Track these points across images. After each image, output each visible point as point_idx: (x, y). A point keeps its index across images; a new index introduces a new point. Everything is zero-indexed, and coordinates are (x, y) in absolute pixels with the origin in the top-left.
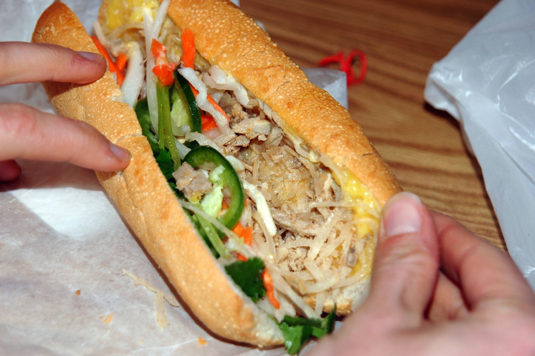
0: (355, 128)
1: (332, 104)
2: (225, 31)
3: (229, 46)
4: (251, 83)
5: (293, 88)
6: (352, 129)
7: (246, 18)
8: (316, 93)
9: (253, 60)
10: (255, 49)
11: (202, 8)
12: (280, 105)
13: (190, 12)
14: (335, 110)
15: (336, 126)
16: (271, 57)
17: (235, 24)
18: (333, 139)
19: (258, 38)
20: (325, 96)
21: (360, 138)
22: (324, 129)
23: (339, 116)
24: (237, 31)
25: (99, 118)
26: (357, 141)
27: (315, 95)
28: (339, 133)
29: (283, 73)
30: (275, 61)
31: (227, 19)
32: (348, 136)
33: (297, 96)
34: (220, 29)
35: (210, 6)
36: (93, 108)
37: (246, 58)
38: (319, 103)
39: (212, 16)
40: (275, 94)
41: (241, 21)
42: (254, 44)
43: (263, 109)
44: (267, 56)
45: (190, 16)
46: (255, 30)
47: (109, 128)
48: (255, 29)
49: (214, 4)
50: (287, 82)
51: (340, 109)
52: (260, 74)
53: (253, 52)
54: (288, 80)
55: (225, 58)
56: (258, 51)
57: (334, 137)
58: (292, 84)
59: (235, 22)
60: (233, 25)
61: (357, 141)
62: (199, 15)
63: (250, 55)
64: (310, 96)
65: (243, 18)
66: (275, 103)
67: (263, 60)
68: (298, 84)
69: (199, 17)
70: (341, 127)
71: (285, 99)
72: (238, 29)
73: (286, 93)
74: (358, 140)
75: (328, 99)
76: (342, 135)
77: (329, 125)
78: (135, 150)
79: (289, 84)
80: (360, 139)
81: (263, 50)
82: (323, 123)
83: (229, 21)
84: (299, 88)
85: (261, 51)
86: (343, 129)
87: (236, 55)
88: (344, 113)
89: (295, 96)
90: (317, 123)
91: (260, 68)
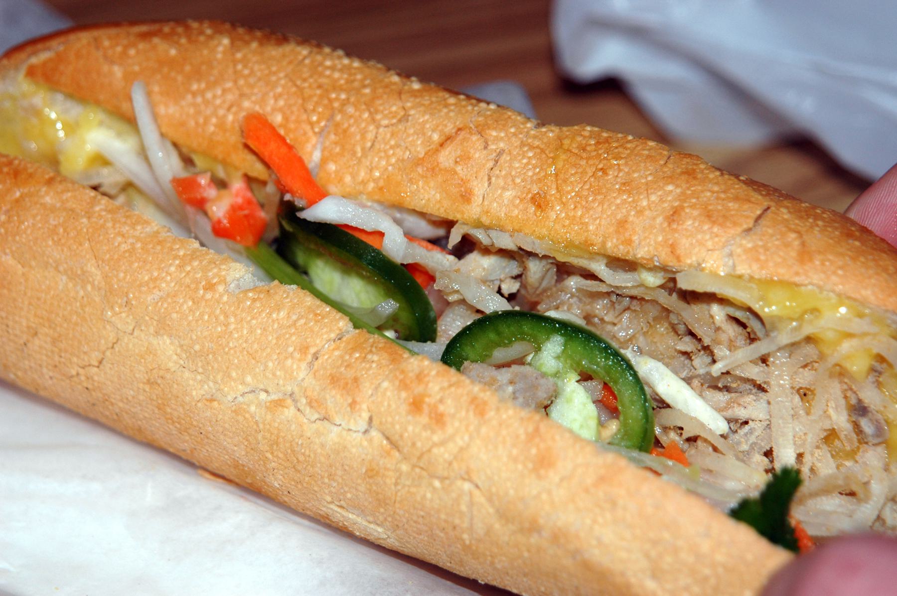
0: (698, 171)
1: (616, 148)
2: (295, 109)
3: (327, 143)
4: (426, 198)
5: (520, 161)
6: (695, 178)
7: (319, 58)
8: (570, 145)
9: (398, 146)
10: (385, 122)
11: (216, 83)
12: (519, 213)
13: (194, 105)
14: (633, 157)
15: (660, 193)
16: (430, 120)
17: (306, 85)
18: (675, 226)
19: (374, 91)
20: (590, 137)
21: (723, 187)
22: (640, 212)
23: (648, 164)
24: (321, 97)
25: (228, 343)
26: (723, 200)
27: (570, 148)
28: (676, 204)
29: (478, 140)
30: (444, 123)
31: (283, 82)
32: (698, 198)
33: (539, 172)
34: (281, 110)
35: (230, 71)
36: (199, 329)
37: (379, 151)
38: (591, 162)
39: (246, 90)
40: (491, 195)
41: (315, 70)
42: (377, 111)
43: (493, 242)
44: (421, 120)
45: (198, 113)
46: (355, 74)
47: (269, 350)
48: (353, 71)
49: (235, 62)
50: (501, 153)
51: (639, 148)
52: (433, 169)
53: (386, 129)
54: (498, 151)
55: (336, 172)
56: (394, 121)
57: (674, 221)
58: (510, 153)
59: (305, 80)
60: (304, 88)
61: (723, 200)
62: (218, 102)
63: (384, 139)
64: (563, 157)
65: (313, 62)
66: (505, 214)
67: (418, 135)
68: (523, 144)
69: (220, 106)
70: (670, 188)
71: (519, 193)
72: (318, 92)
73: (513, 180)
74: (723, 196)
75: (600, 141)
76: (686, 205)
77: (644, 198)
78: (368, 366)
79: (505, 157)
80: (724, 192)
81: (402, 113)
82: (630, 200)
83: (290, 84)
84: (531, 154)
85: (399, 117)
86: (679, 190)
87: (354, 153)
88: (653, 153)
89: (535, 178)
90: (618, 207)
91: (424, 157)
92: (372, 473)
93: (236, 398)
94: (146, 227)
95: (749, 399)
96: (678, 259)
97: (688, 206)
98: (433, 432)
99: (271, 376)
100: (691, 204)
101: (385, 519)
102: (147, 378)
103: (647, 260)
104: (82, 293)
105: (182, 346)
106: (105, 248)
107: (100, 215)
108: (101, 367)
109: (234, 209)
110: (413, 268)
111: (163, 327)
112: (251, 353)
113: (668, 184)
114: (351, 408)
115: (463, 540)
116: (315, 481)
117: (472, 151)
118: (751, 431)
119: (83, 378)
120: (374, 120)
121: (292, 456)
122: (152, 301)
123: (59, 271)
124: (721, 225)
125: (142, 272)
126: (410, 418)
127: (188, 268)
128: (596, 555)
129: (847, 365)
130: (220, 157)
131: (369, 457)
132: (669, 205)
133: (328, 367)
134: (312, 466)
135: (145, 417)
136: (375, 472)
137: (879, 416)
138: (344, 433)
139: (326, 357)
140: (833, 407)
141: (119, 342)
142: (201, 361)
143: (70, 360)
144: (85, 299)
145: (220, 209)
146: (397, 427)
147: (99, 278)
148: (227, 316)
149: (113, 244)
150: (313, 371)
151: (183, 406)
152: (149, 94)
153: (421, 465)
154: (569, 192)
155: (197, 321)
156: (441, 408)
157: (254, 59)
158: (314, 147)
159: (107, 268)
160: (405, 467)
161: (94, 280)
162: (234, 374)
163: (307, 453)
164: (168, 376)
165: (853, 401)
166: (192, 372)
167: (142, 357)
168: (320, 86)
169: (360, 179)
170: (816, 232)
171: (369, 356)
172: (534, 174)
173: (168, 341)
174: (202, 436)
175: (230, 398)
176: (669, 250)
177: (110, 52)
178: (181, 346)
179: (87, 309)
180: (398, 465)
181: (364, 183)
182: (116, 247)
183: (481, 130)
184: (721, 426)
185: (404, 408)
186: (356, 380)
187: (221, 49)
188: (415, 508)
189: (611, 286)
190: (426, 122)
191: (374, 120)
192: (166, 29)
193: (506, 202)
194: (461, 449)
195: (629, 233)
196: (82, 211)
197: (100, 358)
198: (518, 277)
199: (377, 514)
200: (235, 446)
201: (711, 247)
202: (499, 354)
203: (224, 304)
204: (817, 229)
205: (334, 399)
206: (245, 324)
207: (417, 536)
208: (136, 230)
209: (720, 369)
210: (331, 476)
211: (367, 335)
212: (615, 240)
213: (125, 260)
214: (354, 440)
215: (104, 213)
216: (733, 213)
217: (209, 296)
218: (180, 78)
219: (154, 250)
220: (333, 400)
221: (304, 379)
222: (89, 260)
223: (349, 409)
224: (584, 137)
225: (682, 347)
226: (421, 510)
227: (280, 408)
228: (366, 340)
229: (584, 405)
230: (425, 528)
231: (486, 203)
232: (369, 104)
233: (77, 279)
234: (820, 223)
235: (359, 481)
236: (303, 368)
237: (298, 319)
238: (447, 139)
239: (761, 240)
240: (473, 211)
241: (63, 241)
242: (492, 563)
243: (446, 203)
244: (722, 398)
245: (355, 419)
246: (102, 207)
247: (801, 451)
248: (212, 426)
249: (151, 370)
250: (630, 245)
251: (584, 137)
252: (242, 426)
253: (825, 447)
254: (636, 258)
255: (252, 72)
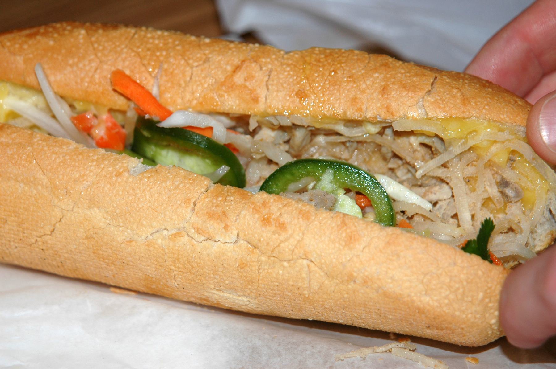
1: (338, 57)
6: (389, 67)
17: (140, 50)
28: (383, 84)
31: (125, 50)
32: (395, 78)
39: (103, 59)
42: (189, 59)
49: (92, 43)
50: (271, 71)
52: (232, 87)
55: (171, 98)
57: (384, 93)
58: (276, 70)
59: (138, 47)
61: (410, 77)
62: (87, 68)
68: (282, 64)
70: (376, 75)
72: (149, 53)
74: (408, 74)
76: (389, 83)
79: (274, 73)
80: (408, 72)
81: (204, 57)
83: (130, 51)
86: (382, 76)
87: (180, 85)
89: (295, 82)
92: (243, 265)
93: (147, 237)
94: (70, 146)
95: (437, 188)
96: (393, 114)
97: (391, 84)
98: (279, 235)
99: (169, 220)
100: (392, 82)
101: (251, 292)
102: (85, 235)
103: (373, 118)
104: (35, 192)
105: (107, 212)
106: (47, 162)
107: (38, 144)
108: (53, 234)
109: (109, 129)
110: (228, 146)
111: (93, 203)
112: (154, 208)
113: (375, 73)
114: (225, 230)
115: (304, 295)
116: (204, 278)
117: (254, 73)
118: (441, 207)
119: (40, 243)
120: (188, 64)
121: (189, 265)
122: (84, 188)
123: (18, 181)
124: (414, 91)
125: (74, 173)
126: (263, 229)
127: (102, 166)
128: (391, 287)
129: (496, 160)
130: (94, 100)
131: (240, 256)
132: (379, 85)
133: (205, 209)
134: (202, 269)
135: (83, 260)
136: (245, 265)
137: (517, 185)
138: (222, 245)
139: (201, 203)
140: (488, 185)
141: (64, 217)
142: (121, 219)
143: (31, 233)
144: (38, 195)
145: (100, 132)
146: (256, 235)
147: (46, 180)
148: (134, 190)
149: (51, 159)
150: (195, 212)
151: (111, 249)
152: (43, 69)
153: (274, 255)
154: (318, 87)
155: (115, 196)
156: (282, 220)
157: (104, 40)
158: (153, 85)
159: (50, 174)
160: (263, 258)
161: (42, 182)
162: (144, 223)
163: (199, 261)
164: (100, 232)
165: (499, 180)
166: (116, 226)
167: (81, 223)
168: (149, 50)
169: (187, 99)
170: (467, 87)
171: (228, 198)
172: (294, 80)
173: (98, 211)
174: (124, 264)
175: (143, 238)
176: (385, 110)
177: (12, 49)
178: (107, 212)
179: (40, 201)
180: (260, 258)
181: (190, 101)
182: (53, 161)
183: (256, 60)
184: (429, 206)
185: (258, 224)
186: (224, 213)
187: (81, 37)
188: (271, 281)
189: (348, 137)
190: (221, 60)
191: (188, 64)
192: (42, 30)
193: (281, 98)
194: (299, 241)
195: (359, 105)
196: (26, 143)
197: (52, 229)
198: (287, 142)
199: (246, 290)
200: (148, 266)
201: (410, 105)
202: (292, 186)
203: (130, 183)
204: (466, 85)
205: (213, 227)
206: (147, 193)
207: (272, 298)
208: (64, 149)
209: (421, 173)
210: (215, 273)
211: (222, 186)
212: (351, 110)
213: (61, 167)
214: (229, 248)
215: (40, 142)
216: (417, 83)
217: (119, 180)
218: (60, 58)
219: (78, 159)
220: (212, 227)
221: (190, 218)
222: (37, 171)
223: (224, 230)
224: (317, 54)
225: (391, 165)
226: (276, 282)
227: (178, 238)
228: (223, 190)
229: (352, 206)
230: (279, 292)
231: (268, 101)
232: (183, 55)
233: (31, 184)
234: (466, 81)
235: (234, 272)
236: (189, 212)
237: (179, 184)
238: (237, 68)
239: (438, 96)
240: (261, 107)
241: (19, 162)
242: (323, 305)
243: (243, 106)
244: (422, 190)
245: (228, 236)
246: (39, 139)
247: (473, 213)
248: (132, 257)
249: (88, 230)
250: (361, 111)
251: (317, 54)
252: (153, 253)
253: (484, 209)
254: (366, 118)
255: (104, 48)
